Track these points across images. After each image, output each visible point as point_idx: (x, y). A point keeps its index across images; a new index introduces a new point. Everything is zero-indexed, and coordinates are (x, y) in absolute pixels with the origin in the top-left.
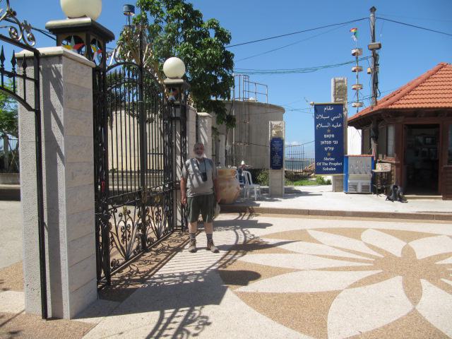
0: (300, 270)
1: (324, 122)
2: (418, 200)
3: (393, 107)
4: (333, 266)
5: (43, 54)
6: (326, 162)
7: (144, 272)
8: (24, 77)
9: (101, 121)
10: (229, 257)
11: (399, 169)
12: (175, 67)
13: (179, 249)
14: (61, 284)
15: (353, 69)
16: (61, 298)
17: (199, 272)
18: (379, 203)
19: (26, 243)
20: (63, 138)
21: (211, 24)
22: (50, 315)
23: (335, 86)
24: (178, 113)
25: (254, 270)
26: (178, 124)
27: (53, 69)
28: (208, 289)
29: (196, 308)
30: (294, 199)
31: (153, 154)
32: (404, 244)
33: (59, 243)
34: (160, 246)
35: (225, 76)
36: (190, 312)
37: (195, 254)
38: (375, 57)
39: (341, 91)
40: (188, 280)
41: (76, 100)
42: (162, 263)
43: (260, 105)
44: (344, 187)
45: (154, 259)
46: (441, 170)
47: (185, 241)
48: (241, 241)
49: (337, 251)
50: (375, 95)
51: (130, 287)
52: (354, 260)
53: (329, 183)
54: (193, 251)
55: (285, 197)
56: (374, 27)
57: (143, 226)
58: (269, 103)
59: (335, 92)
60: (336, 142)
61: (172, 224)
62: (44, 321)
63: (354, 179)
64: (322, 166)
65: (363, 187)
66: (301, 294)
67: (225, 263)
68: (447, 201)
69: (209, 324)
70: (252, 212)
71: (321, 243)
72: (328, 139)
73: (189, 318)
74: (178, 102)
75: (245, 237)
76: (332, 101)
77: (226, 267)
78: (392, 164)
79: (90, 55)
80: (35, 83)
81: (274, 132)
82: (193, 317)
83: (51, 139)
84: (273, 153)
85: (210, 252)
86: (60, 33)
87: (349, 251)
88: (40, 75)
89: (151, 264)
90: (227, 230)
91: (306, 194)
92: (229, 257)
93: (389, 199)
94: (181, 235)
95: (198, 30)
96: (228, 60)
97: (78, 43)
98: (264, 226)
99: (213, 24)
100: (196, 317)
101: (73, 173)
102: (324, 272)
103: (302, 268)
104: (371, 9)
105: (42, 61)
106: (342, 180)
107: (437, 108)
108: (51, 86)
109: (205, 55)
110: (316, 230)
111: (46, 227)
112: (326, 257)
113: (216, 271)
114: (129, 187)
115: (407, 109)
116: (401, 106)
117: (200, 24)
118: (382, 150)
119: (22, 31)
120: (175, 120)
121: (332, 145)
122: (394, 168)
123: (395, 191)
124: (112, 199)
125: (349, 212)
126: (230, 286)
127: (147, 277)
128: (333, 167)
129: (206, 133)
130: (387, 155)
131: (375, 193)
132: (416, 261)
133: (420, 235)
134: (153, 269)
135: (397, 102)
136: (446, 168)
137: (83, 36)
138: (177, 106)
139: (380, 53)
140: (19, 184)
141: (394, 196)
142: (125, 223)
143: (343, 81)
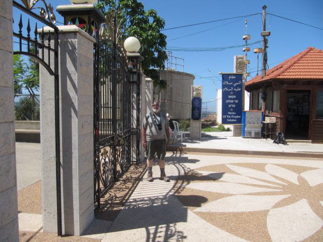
0: (234, 195)
1: (229, 87)
2: (294, 143)
3: (280, 77)
4: (255, 192)
5: (62, 31)
6: (230, 115)
7: (121, 197)
8: (49, 48)
9: (97, 83)
10: (178, 185)
11: (282, 121)
12: (133, 45)
13: (139, 179)
14: (73, 209)
15: (244, 49)
16: (73, 219)
17: (161, 197)
18: (268, 145)
19: (45, 178)
20: (77, 97)
21: (151, 13)
22: (63, 233)
23: (237, 61)
24: (135, 78)
25: (200, 194)
26: (135, 87)
27: (69, 42)
28: (176, 208)
29: (171, 225)
30: (208, 142)
31: (109, 107)
32: (298, 175)
33: (72, 177)
34: (124, 177)
35: (159, 52)
36: (168, 228)
37: (152, 183)
38: (265, 41)
39: (241, 65)
40: (156, 203)
41: (85, 67)
42: (132, 190)
43: (179, 73)
44: (242, 133)
45: (124, 187)
46: (311, 122)
47: (142, 173)
48: (182, 173)
49: (253, 180)
50: (265, 69)
51: (115, 209)
52: (268, 187)
53: (228, 130)
54: (151, 181)
55: (202, 140)
56: (265, 20)
57: (114, 163)
58: (185, 72)
59: (237, 66)
60: (237, 101)
61: (129, 159)
62: (60, 237)
63: (250, 127)
64: (226, 118)
65: (256, 133)
66: (242, 213)
67: (178, 190)
68: (314, 144)
69: (185, 237)
70: (181, 151)
71: (240, 174)
72: (231, 99)
73: (169, 233)
74: (135, 70)
75: (184, 170)
76: (235, 72)
77: (179, 193)
78: (277, 117)
79: (90, 32)
80: (55, 53)
81: (195, 93)
82: (171, 232)
83: (66, 97)
84: (193, 109)
85: (163, 181)
86: (69, 15)
87: (262, 180)
88: (59, 49)
89: (123, 191)
90: (169, 164)
91: (215, 138)
92: (178, 185)
93: (275, 142)
94: (137, 169)
95: (140, 17)
96: (162, 40)
97: (82, 23)
98: (194, 161)
99: (152, 13)
100: (173, 232)
101: (82, 124)
102: (251, 196)
103: (234, 193)
104: (263, 7)
105: (60, 36)
106: (241, 128)
107: (311, 79)
108: (67, 56)
109: (148, 36)
110: (232, 164)
111: (62, 165)
112: (248, 184)
113: (173, 195)
114: (107, 132)
115: (290, 79)
116: (286, 77)
117: (143, 13)
118: (269, 108)
119: (48, 11)
120: (131, 83)
121: (234, 103)
122: (279, 120)
123: (279, 137)
124: (103, 141)
125: (250, 152)
126: (189, 207)
127: (124, 201)
128: (234, 119)
129: (150, 93)
130: (272, 111)
131: (264, 138)
132: (310, 188)
133: (305, 169)
134: (127, 194)
135: (283, 74)
136: (314, 121)
137: (86, 18)
138: (135, 73)
139: (269, 38)
140: (39, 129)
141: (279, 141)
142: (105, 160)
143: (242, 58)
